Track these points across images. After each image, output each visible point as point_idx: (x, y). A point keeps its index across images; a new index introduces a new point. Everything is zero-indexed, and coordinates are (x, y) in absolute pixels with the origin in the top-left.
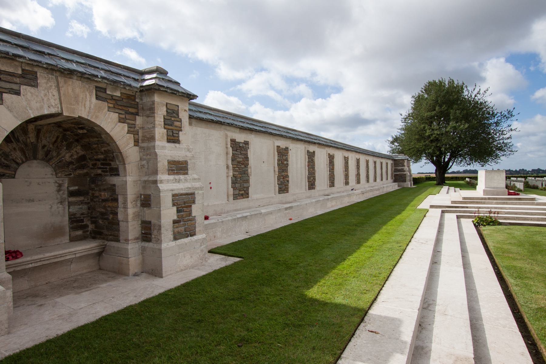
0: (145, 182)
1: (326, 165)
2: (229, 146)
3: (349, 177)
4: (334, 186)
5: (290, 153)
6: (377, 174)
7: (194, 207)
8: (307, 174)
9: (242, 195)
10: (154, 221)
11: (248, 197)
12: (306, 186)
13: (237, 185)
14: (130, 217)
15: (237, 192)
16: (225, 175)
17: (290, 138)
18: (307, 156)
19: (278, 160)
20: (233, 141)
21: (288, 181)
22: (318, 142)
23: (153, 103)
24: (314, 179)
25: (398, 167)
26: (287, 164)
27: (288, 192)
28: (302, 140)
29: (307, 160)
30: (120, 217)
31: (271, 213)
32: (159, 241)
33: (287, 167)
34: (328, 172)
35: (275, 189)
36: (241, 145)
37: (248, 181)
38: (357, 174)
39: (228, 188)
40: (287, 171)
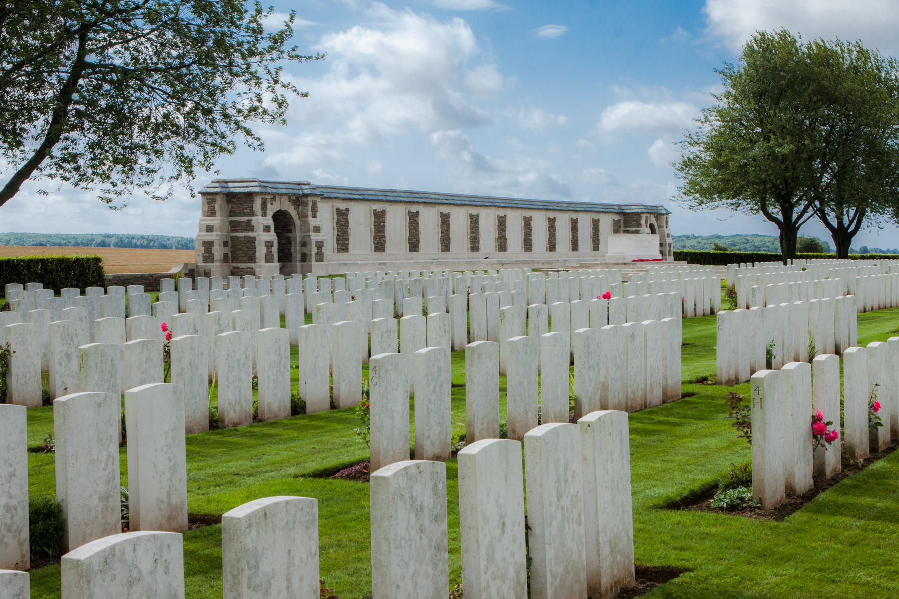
0: (304, 236)
1: (436, 226)
2: (335, 213)
3: (479, 240)
4: (448, 250)
5: (387, 215)
6: (557, 237)
7: (323, 248)
8: (408, 235)
9: (343, 249)
10: (307, 253)
11: (347, 252)
12: (406, 247)
13: (340, 242)
14: (298, 251)
15: (340, 247)
16: (332, 234)
17: (387, 201)
18: (408, 217)
19: (375, 222)
20: (338, 209)
21: (384, 241)
22: (423, 200)
23: (308, 201)
24: (418, 240)
25: (631, 227)
26: (384, 225)
27: (384, 251)
28: (400, 202)
29: (408, 221)
30: (292, 250)
31: (365, 264)
32: (310, 261)
33: (384, 228)
34: (440, 234)
35: (371, 247)
36: (343, 212)
37: (347, 239)
38: (500, 238)
39: (333, 244)
40: (383, 232)
